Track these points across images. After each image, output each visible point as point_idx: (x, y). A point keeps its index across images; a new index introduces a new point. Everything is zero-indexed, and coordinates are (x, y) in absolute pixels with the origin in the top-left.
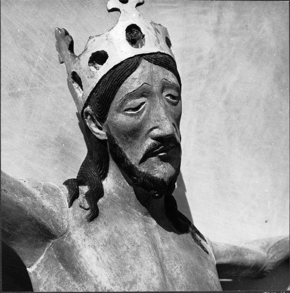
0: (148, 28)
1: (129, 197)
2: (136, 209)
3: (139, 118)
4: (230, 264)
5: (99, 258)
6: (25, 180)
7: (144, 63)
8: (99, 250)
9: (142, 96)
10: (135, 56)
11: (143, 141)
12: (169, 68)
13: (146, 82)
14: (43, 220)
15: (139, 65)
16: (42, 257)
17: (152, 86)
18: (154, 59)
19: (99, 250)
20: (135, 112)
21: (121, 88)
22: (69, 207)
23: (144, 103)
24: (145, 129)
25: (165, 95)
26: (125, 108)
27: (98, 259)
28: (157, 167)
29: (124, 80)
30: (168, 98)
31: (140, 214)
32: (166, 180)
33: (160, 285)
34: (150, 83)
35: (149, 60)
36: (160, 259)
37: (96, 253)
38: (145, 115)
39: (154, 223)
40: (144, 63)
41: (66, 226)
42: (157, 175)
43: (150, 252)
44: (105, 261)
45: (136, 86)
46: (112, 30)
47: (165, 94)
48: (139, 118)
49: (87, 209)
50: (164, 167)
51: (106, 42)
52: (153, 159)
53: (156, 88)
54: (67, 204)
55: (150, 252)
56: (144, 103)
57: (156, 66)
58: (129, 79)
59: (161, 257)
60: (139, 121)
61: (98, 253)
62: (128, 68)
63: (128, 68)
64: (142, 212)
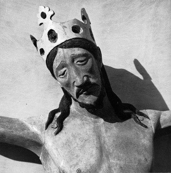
0: (59, 28)
1: (84, 112)
2: (89, 117)
3: (66, 78)
4: (156, 127)
5: (59, 154)
6: (26, 120)
7: (60, 50)
8: (59, 150)
9: (63, 67)
10: (54, 48)
11: (73, 89)
12: (75, 46)
13: (62, 60)
14: (34, 139)
15: (57, 52)
16: (42, 153)
17: (66, 61)
18: (64, 46)
19: (59, 150)
20: (63, 76)
21: (54, 66)
22: (46, 130)
23: (66, 70)
24: (71, 83)
25: (76, 62)
26: (59, 75)
27: (58, 155)
28: (85, 99)
29: (53, 62)
30: (79, 63)
31: (92, 119)
32: (93, 104)
33: (96, 161)
34: (64, 61)
35: (62, 47)
36: (59, 169)
37: (57, 152)
38: (69, 76)
39: (102, 121)
40: (60, 50)
41: (44, 141)
42: (87, 103)
43: (94, 142)
44: (62, 155)
45: (58, 64)
46: (42, 36)
47: (75, 62)
48: (66, 78)
49: (56, 128)
50: (89, 98)
51: (41, 43)
52: (82, 95)
53: (68, 62)
54: (45, 128)
55: (94, 142)
56: (66, 70)
57: (66, 49)
58: (55, 61)
59: (102, 141)
60: (67, 80)
61: (58, 152)
62: (53, 56)
63: (53, 56)
64: (93, 118)
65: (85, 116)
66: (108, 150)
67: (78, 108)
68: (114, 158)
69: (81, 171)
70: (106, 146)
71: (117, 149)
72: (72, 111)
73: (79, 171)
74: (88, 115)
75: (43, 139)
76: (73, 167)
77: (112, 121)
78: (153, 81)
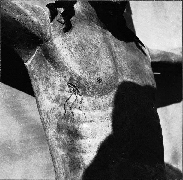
2: (97, 24)
5: (72, 56)
8: (72, 50)
16: (34, 56)
37: (70, 53)
41: (50, 35)
61: (72, 53)
65: (93, 22)
66: (120, 66)
67: (86, 10)
68: (128, 76)
69: (101, 80)
70: (118, 62)
71: (129, 67)
72: (77, 11)
73: (99, 80)
74: (96, 21)
75: (49, 33)
76: (93, 74)
77: (119, 38)
78: (133, 16)
